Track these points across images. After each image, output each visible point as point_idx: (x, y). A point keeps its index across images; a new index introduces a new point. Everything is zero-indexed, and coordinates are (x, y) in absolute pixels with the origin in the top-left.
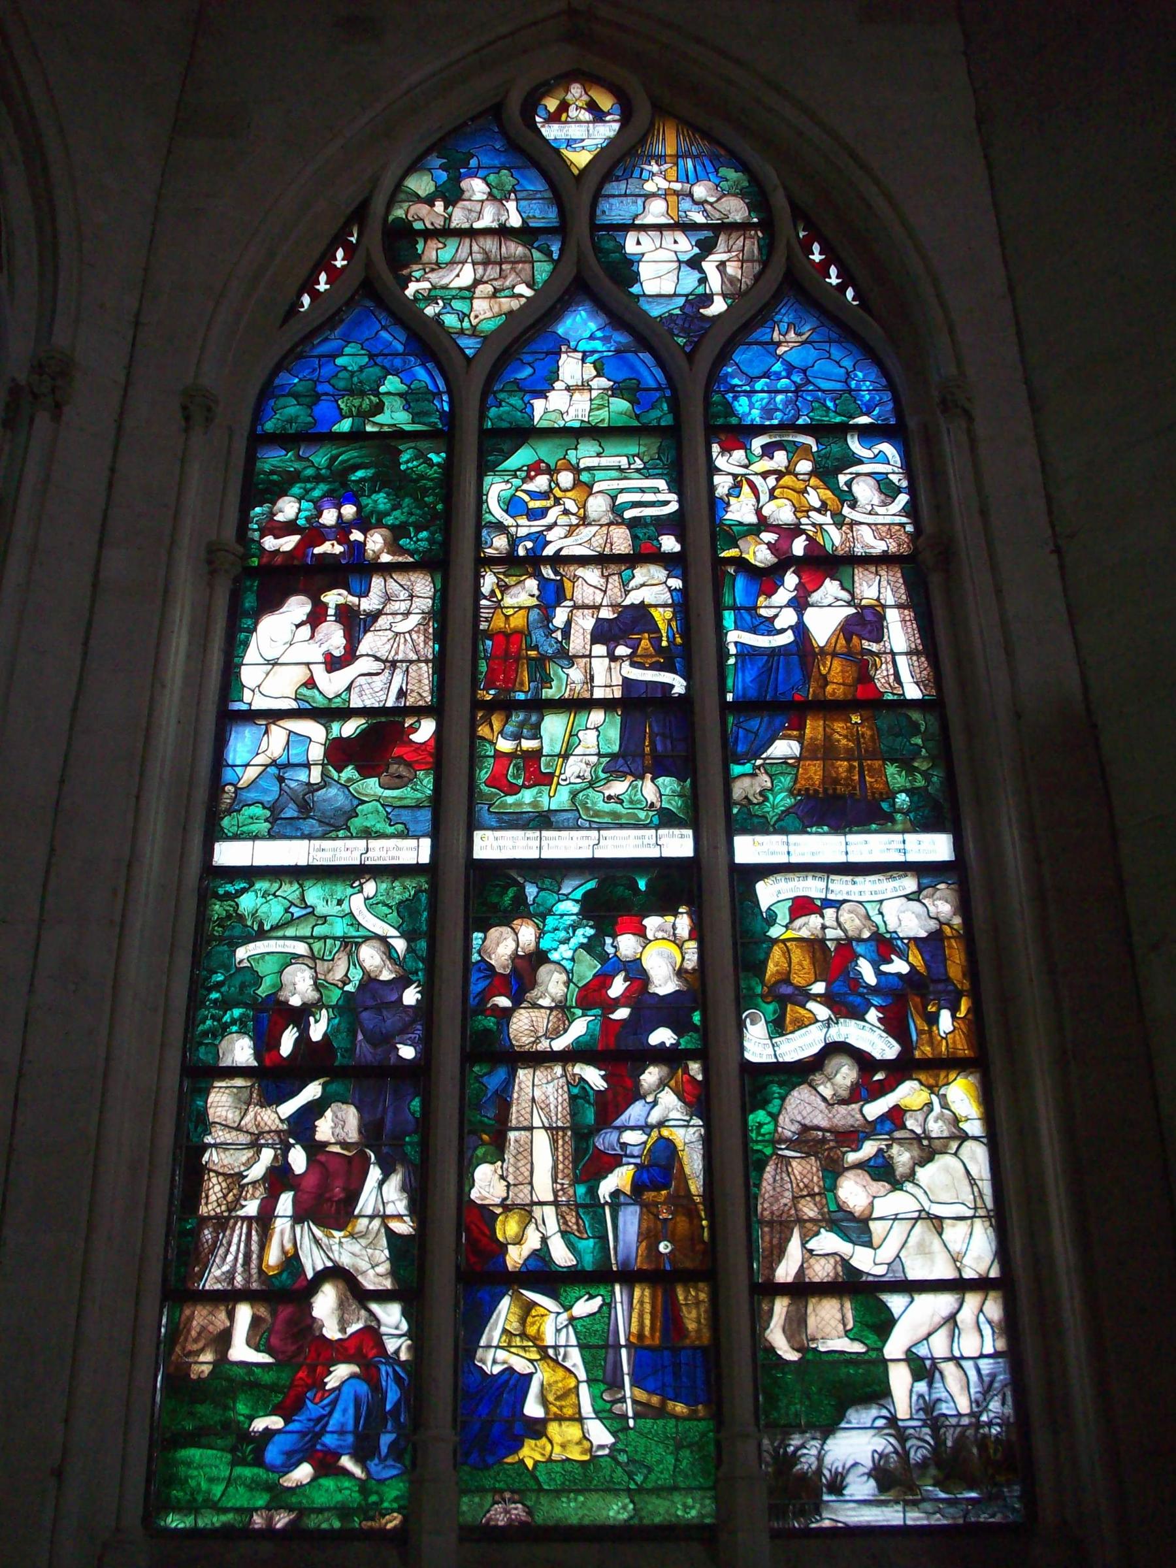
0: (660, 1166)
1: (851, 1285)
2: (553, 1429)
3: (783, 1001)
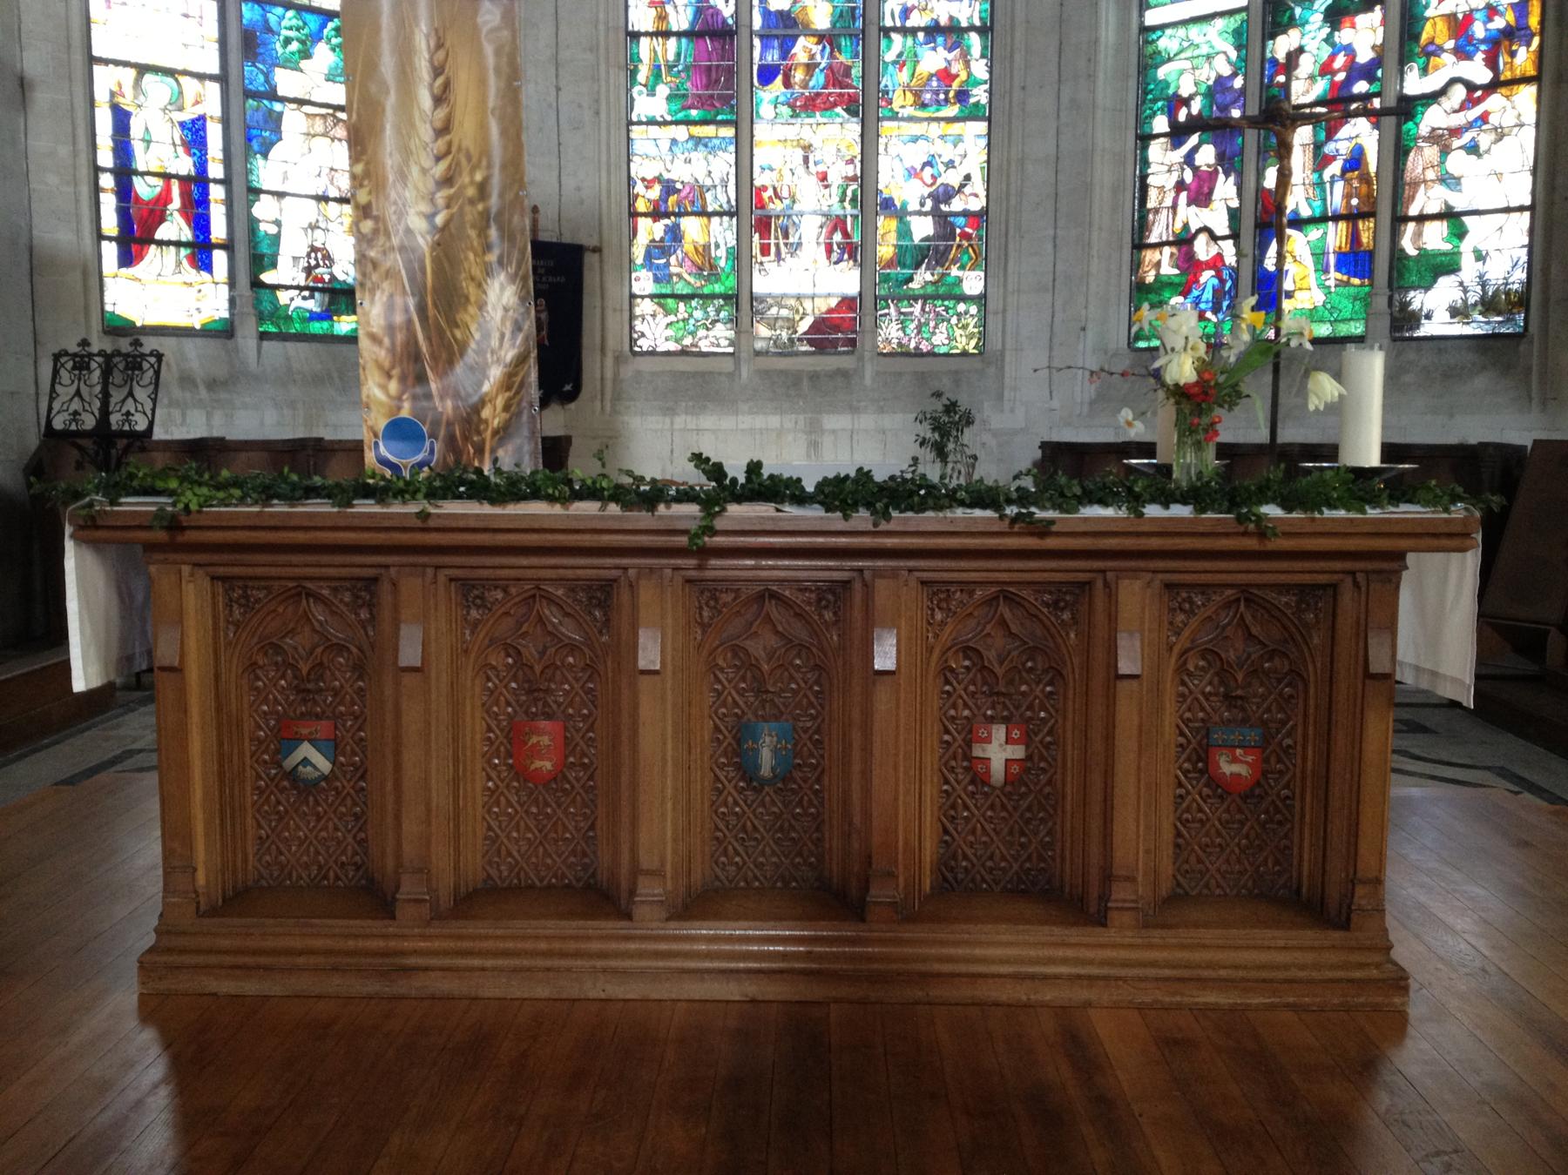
0: (1355, 161)
1: (1449, 215)
2: (1297, 294)
3: (1428, 55)
